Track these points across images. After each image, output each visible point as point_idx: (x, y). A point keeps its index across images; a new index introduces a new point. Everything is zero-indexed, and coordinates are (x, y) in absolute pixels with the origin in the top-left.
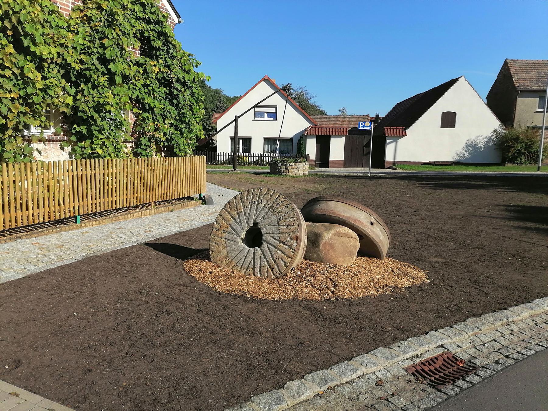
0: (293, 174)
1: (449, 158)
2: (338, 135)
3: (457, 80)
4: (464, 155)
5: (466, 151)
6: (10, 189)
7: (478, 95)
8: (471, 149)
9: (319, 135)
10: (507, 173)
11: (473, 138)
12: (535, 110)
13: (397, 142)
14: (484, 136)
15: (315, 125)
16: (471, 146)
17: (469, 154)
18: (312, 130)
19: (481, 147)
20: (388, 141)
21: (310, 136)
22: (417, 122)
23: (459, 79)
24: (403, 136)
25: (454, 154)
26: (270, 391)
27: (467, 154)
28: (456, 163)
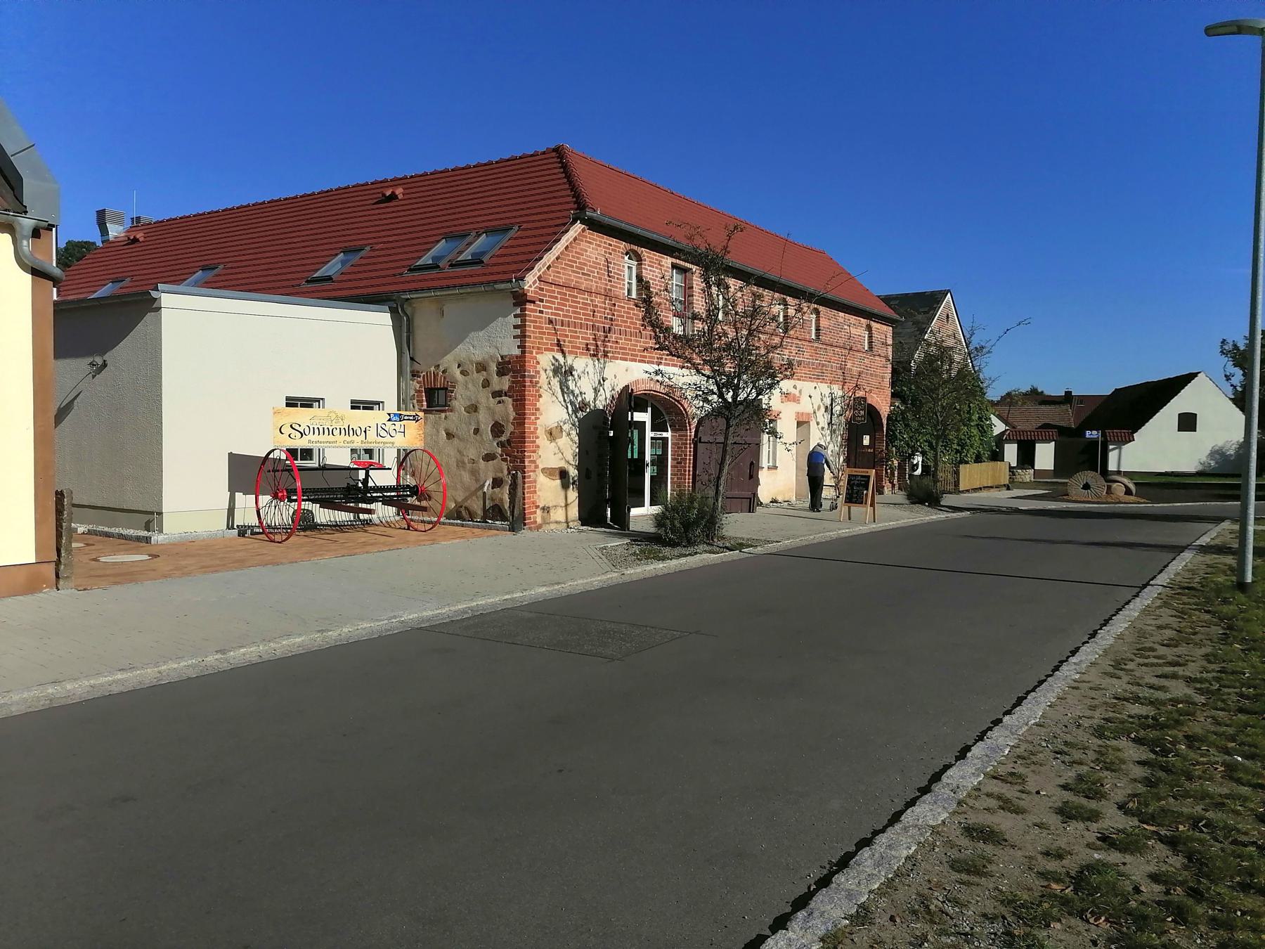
0: (1021, 480)
1: (1192, 468)
2: (1046, 439)
3: (1190, 377)
4: (1210, 464)
5: (1211, 460)
6: (958, 479)
7: (1224, 393)
8: (1218, 457)
9: (1024, 440)
10: (1171, 504)
11: (1220, 443)
12: (113, 222)
13: (1120, 449)
14: (1234, 441)
15: (1014, 428)
16: (1217, 453)
17: (1216, 463)
18: (1011, 433)
19: (1231, 455)
20: (1111, 447)
21: (1010, 441)
22: (1147, 424)
23: (1199, 375)
24: (1130, 441)
25: (1196, 463)
26: (1188, 644)
27: (1213, 463)
28: (1199, 474)
